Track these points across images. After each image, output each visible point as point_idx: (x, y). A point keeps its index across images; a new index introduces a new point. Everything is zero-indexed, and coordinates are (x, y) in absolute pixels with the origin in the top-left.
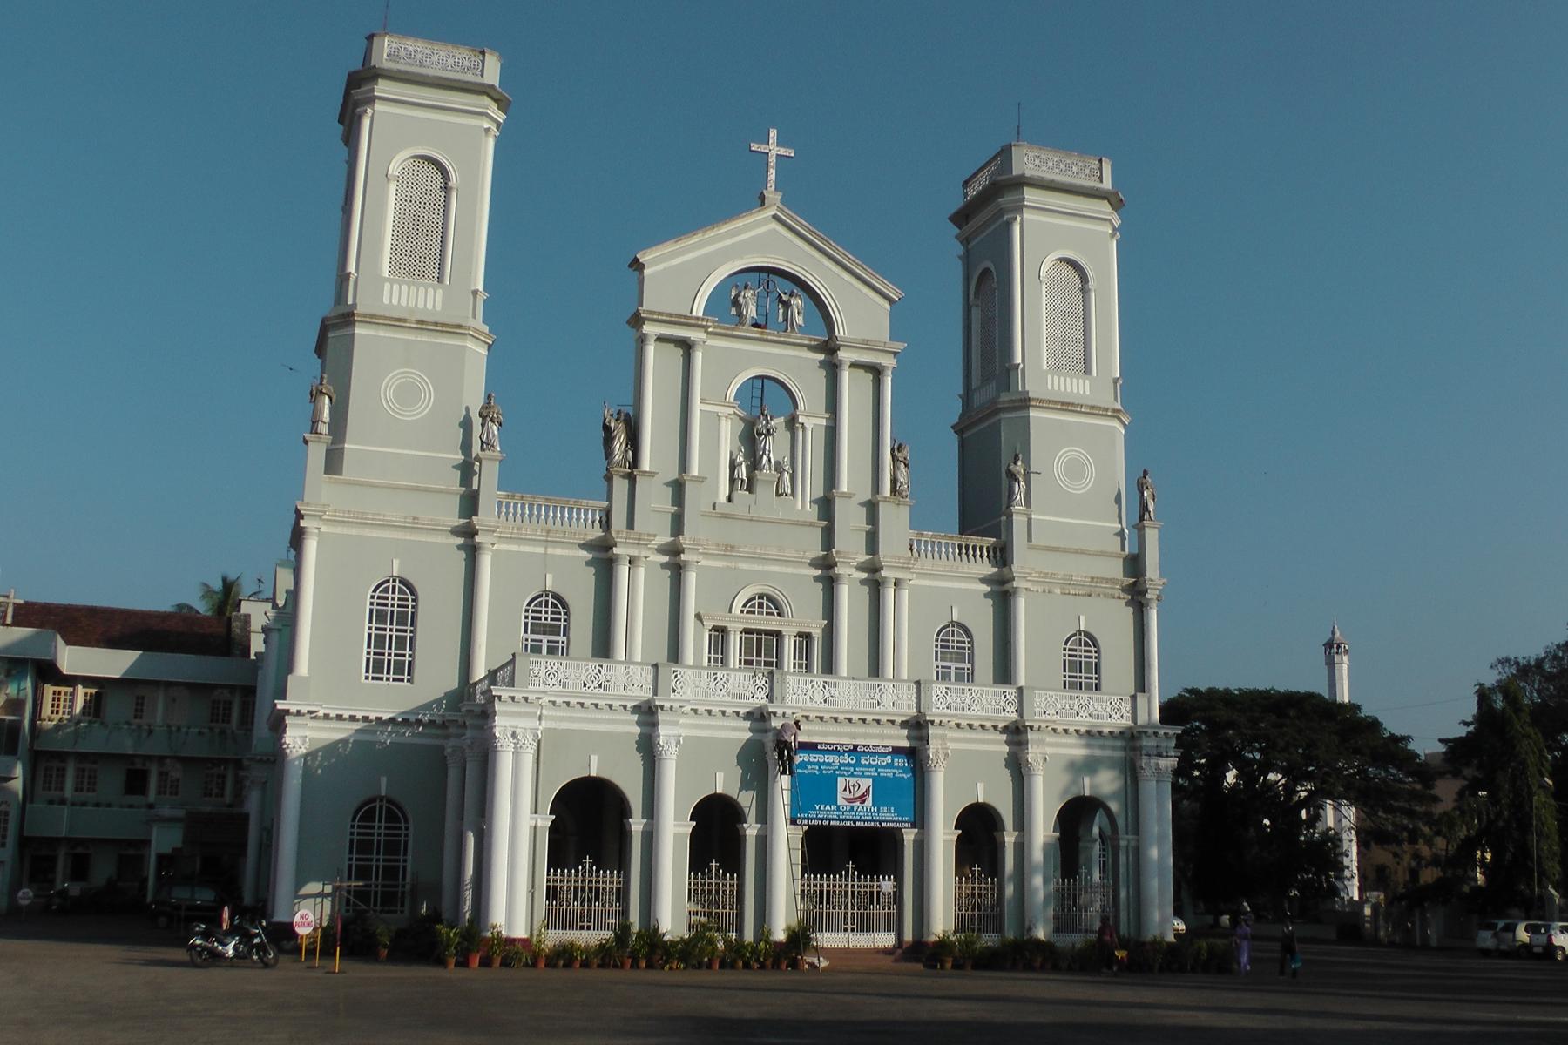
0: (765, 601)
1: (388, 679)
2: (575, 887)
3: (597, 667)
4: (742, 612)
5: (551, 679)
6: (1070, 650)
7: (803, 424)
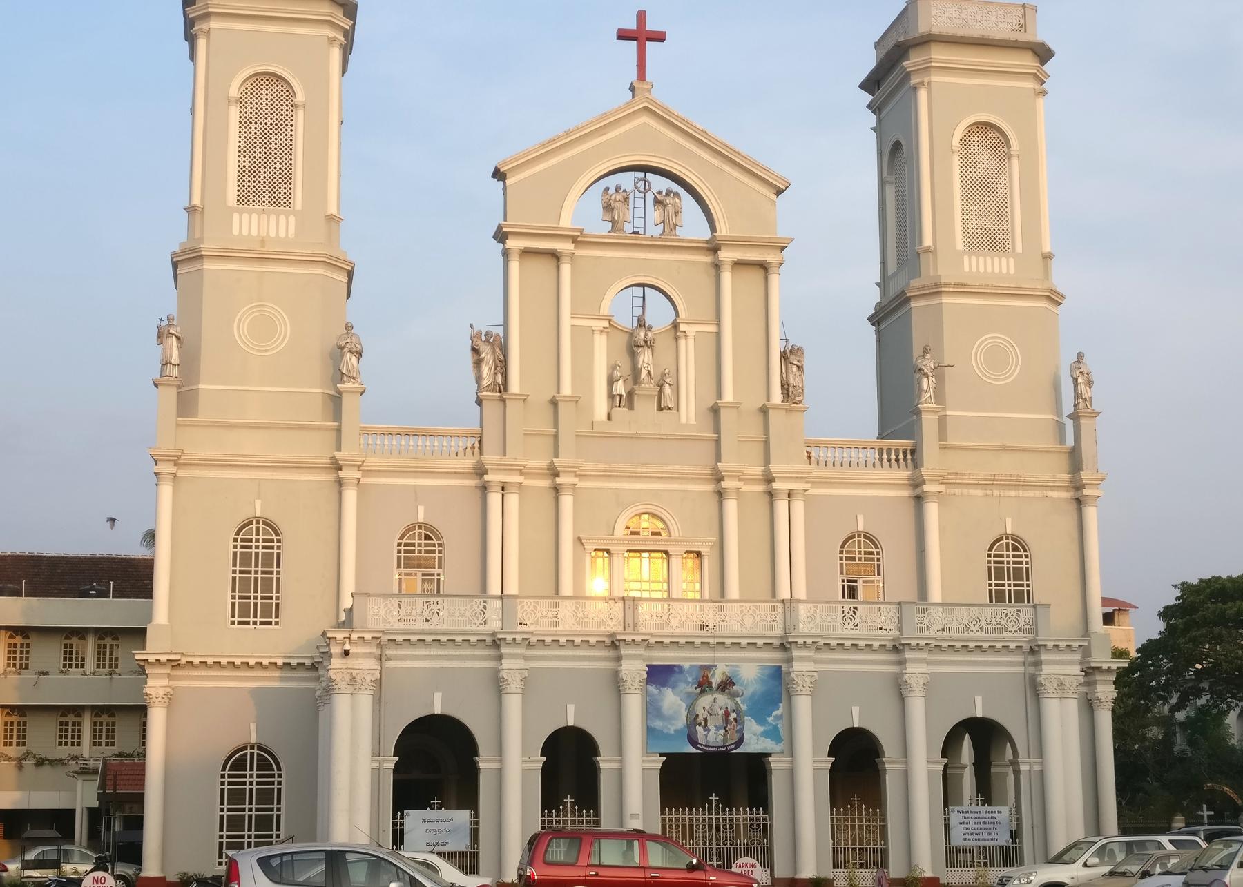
1: (255, 623)
3: (813, 608)
5: (974, 625)
6: (995, 556)
7: (685, 332)
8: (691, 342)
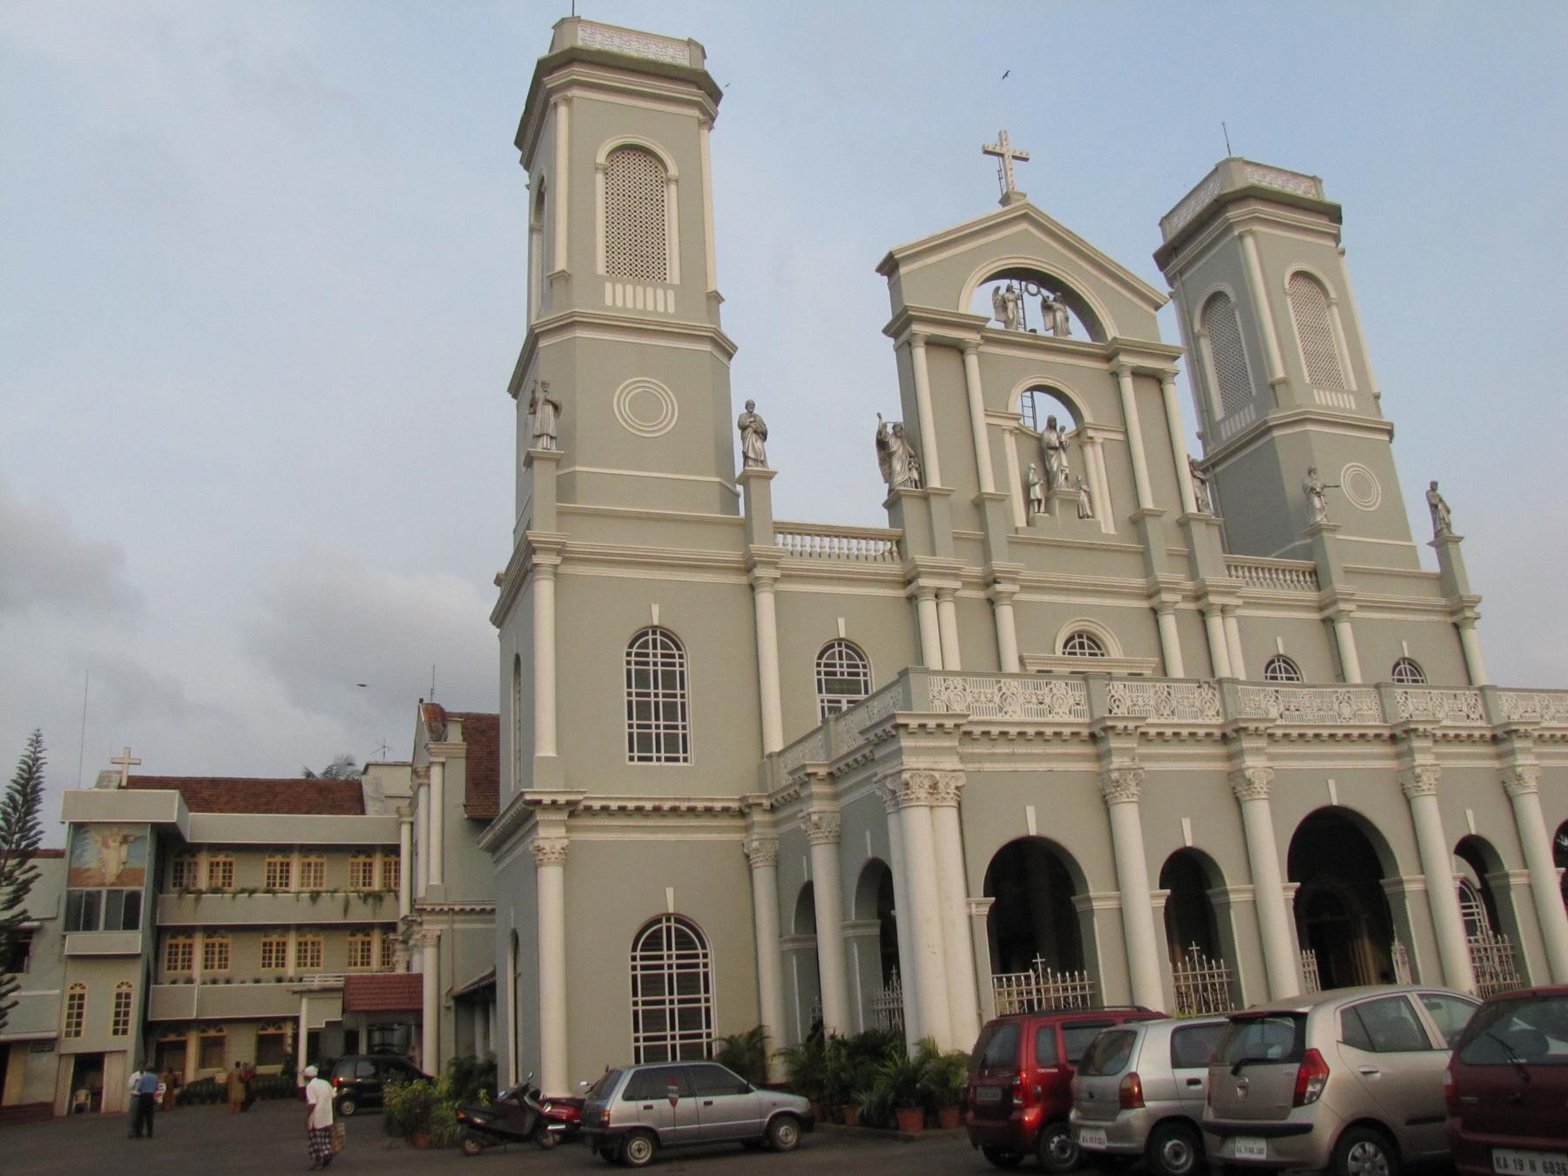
0: (1085, 641)
2: (1046, 999)
4: (1064, 653)
8: (1099, 448)
